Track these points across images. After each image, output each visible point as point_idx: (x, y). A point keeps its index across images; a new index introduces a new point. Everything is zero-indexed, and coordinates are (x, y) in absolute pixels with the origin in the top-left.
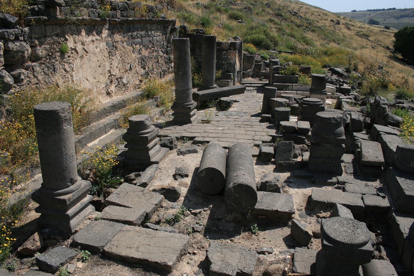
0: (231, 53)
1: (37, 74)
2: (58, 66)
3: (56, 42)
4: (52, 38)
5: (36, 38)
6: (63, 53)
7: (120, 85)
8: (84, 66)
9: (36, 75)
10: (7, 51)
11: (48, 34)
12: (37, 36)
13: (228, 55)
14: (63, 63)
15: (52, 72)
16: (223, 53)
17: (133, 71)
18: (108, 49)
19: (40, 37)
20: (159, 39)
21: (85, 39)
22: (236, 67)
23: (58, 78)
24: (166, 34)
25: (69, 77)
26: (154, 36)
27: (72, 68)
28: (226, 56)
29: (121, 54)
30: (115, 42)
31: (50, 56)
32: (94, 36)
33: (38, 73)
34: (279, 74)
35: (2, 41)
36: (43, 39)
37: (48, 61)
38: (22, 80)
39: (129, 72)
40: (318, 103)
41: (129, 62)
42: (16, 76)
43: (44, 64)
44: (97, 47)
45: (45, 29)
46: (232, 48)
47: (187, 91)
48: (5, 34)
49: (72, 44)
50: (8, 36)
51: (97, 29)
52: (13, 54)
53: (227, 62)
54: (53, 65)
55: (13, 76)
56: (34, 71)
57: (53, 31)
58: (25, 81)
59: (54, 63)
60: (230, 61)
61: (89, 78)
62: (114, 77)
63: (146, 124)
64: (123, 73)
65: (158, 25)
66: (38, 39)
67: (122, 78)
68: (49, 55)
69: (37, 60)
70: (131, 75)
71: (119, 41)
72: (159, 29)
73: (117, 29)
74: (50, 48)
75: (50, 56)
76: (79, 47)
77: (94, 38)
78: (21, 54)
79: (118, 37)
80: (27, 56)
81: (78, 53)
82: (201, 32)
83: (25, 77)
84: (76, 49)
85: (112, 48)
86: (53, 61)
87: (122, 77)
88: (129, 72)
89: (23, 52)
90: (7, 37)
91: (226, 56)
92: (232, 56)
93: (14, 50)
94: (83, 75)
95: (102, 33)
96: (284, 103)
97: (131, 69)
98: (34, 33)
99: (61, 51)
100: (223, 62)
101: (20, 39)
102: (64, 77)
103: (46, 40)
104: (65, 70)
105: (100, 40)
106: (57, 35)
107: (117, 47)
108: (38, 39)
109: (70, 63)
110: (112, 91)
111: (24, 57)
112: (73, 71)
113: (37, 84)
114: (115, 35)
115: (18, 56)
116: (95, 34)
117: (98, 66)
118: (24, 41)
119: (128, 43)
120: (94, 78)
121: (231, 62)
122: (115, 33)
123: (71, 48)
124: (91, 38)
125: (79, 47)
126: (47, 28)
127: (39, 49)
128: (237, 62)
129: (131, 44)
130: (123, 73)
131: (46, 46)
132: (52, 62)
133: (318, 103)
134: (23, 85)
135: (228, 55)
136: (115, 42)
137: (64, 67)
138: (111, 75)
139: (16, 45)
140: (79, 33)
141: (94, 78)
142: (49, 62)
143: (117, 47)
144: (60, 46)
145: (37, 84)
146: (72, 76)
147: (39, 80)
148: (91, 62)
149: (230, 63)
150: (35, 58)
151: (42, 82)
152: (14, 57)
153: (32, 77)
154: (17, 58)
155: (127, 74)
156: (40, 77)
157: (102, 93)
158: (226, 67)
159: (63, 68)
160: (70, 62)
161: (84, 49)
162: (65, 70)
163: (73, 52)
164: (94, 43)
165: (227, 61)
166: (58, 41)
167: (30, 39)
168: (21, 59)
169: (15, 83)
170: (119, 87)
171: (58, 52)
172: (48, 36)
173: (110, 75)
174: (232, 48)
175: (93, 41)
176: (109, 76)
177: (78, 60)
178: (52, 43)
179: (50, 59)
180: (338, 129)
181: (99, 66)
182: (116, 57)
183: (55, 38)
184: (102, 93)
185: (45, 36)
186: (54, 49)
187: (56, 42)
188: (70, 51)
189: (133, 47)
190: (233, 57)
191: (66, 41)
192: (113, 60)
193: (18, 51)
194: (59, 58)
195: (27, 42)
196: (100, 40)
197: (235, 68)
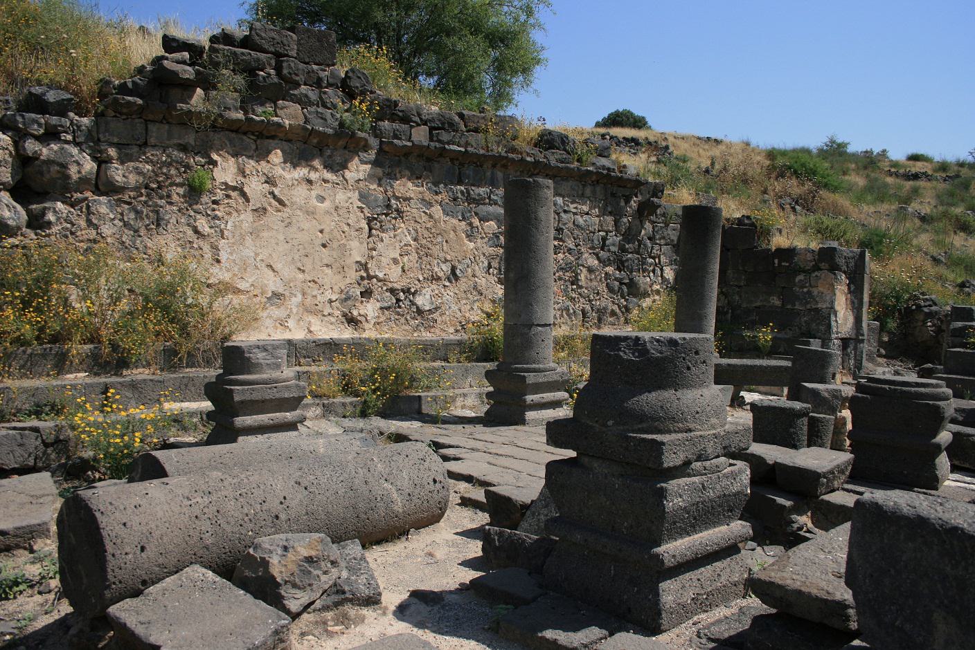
0: (820, 281)
1: (99, 220)
2: (170, 213)
3: (177, 162)
4: (164, 151)
5: (112, 144)
6: (194, 192)
7: (400, 307)
8: (265, 234)
9: (95, 221)
10: (23, 161)
11: (152, 141)
12: (116, 140)
13: (810, 286)
14: (192, 213)
15: (148, 225)
16: (797, 280)
17: (463, 284)
18: (366, 211)
19: (128, 145)
20: (586, 221)
21: (278, 171)
22: (833, 324)
23: (168, 244)
24: (617, 214)
25: (206, 248)
26: (565, 211)
27: (222, 231)
28: (805, 290)
29: (416, 231)
30: (397, 198)
31: (153, 189)
32: (316, 170)
33: (101, 217)
34: (964, 345)
35: (10, 134)
36: (136, 149)
37: (143, 199)
38: (49, 224)
39: (447, 284)
40: (922, 390)
41: (449, 258)
42: (35, 212)
43: (129, 203)
44: (322, 199)
45: (147, 129)
46: (822, 265)
47: (526, 330)
48: (16, 120)
49: (231, 176)
50: (24, 124)
51: (330, 157)
52: (40, 166)
53: (808, 307)
54: (157, 212)
55: (29, 212)
56: (89, 212)
57: (170, 136)
58: (55, 229)
59: (161, 207)
60: (817, 303)
61: (278, 266)
62: (379, 284)
63: (249, 359)
64: (419, 281)
65: (584, 186)
66: (118, 146)
67: (414, 294)
68: (147, 187)
69: (111, 191)
70: (452, 294)
71: (411, 198)
72: (589, 198)
73: (410, 168)
74: (153, 171)
75: (153, 189)
76: (255, 187)
77: (314, 176)
78: (57, 168)
79: (406, 187)
80: (78, 176)
81: (248, 200)
82: (746, 221)
83: (58, 219)
84: (242, 188)
85: (381, 215)
86: (162, 202)
87: (413, 290)
88: (447, 284)
89: (64, 166)
90: (21, 126)
91: (805, 290)
92: (821, 289)
93: (42, 157)
94: (257, 255)
95: (347, 168)
96: (826, 395)
97: (454, 276)
98: (107, 131)
99: (189, 186)
100: (797, 307)
101: (63, 138)
102: (188, 246)
103: (144, 154)
104: (196, 231)
105: (337, 184)
106: (184, 148)
107: (403, 212)
108: (120, 146)
109: (216, 218)
110: (365, 316)
111: (68, 177)
112: (224, 238)
113: (95, 241)
114: (398, 182)
115: (49, 171)
116: (320, 167)
117: (319, 242)
118: (77, 144)
119: (448, 209)
120: (299, 269)
121: (819, 306)
122: (398, 175)
123: (226, 184)
124: (302, 172)
125: (253, 186)
126: (153, 128)
127: (117, 169)
128: (837, 307)
129: (463, 215)
130: (419, 281)
131: (141, 165)
132: (157, 205)
133: (922, 390)
134: (48, 236)
135: (810, 286)
136: (397, 198)
137: (192, 221)
138: (370, 277)
139: (51, 149)
140: (261, 155)
141: (299, 269)
142: (145, 202)
143: (403, 212)
144: (189, 174)
145: (95, 241)
146: (215, 248)
147: (101, 234)
148: (293, 229)
149: (817, 310)
150: (103, 185)
151: (109, 240)
152: (42, 174)
153: (83, 223)
154: (48, 176)
155: (434, 287)
156: (107, 230)
157: (326, 313)
158: (805, 322)
159: (188, 225)
160: (216, 215)
161: (272, 193)
162: (196, 231)
163: (234, 194)
164: (313, 187)
165: (807, 303)
166: (183, 162)
167: (92, 142)
168: (60, 181)
169: (29, 226)
170: (398, 314)
171: (181, 185)
172: (154, 146)
173: (365, 275)
174: (822, 265)
175: (310, 182)
176: (362, 278)
177: (247, 218)
178: (162, 162)
179: (148, 195)
180: (644, 397)
181: (324, 246)
182: (395, 236)
183: (175, 153)
184: (326, 313)
185: (146, 144)
186: (168, 177)
187: (177, 162)
188: (221, 190)
189: (471, 224)
190: (825, 291)
191: (211, 167)
192: (382, 241)
193: (49, 162)
194: (182, 200)
195: (84, 147)
196: (337, 184)
197: (829, 326)
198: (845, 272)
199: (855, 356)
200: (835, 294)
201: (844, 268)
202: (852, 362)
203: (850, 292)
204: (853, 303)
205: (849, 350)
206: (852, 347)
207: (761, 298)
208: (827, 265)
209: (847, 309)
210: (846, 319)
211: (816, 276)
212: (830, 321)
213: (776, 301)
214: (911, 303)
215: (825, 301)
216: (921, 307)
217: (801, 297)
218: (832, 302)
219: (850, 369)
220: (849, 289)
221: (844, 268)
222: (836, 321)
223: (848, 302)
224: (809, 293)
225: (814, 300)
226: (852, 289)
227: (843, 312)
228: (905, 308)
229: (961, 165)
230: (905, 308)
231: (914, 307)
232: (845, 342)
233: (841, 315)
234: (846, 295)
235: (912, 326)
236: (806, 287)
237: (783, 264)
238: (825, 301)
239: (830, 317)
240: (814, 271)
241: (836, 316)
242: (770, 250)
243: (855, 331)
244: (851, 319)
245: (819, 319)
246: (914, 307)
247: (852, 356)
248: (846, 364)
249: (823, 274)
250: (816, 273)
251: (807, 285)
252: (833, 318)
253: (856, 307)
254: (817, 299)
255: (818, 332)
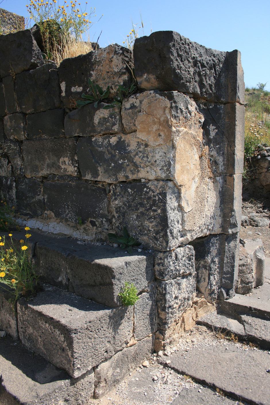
0: (141, 117)
16: (96, 120)
22: (173, 215)
28: (113, 140)
46: (143, 80)
53: (121, 177)
91: (113, 140)
92: (142, 136)
100: (103, 178)
121: (142, 174)
128: (180, 177)
149: (138, 185)
165: (119, 168)
174: (143, 80)
190: (151, 140)
197: (164, 222)
198: (195, 97)
199: (221, 267)
200: (174, 147)
201: (194, 87)
202: (215, 279)
203: (208, 141)
204: (214, 163)
205: (209, 259)
206: (214, 250)
207: (48, 161)
208: (152, 77)
209: (202, 178)
210: (201, 200)
211: (133, 107)
212: (164, 211)
213: (69, 167)
214: (256, 153)
215: (153, 164)
216: (265, 156)
217: (107, 156)
218: (169, 166)
219: (213, 292)
220: (206, 133)
221: (194, 87)
222: (180, 208)
223: (206, 162)
224: (121, 146)
225: (131, 160)
226: (212, 134)
227: (194, 186)
228: (252, 158)
229: (254, 90)
230: (252, 158)
231: (259, 157)
232: (201, 246)
233: (189, 194)
234: (200, 147)
235: (258, 172)
236: (114, 134)
237: (73, 89)
238: (153, 164)
239: (163, 202)
240: (125, 96)
241: (179, 198)
242: (52, 66)
243: (220, 220)
244: (212, 198)
245: (142, 205)
246: (259, 157)
247: (215, 267)
248: (203, 285)
249: (148, 100)
250: (132, 100)
251: (116, 128)
252: (171, 202)
253: (220, 172)
254: (137, 160)
255: (141, 233)
